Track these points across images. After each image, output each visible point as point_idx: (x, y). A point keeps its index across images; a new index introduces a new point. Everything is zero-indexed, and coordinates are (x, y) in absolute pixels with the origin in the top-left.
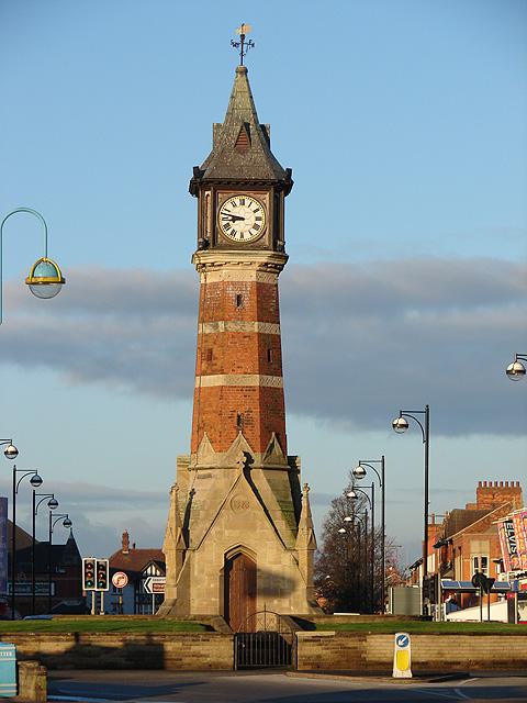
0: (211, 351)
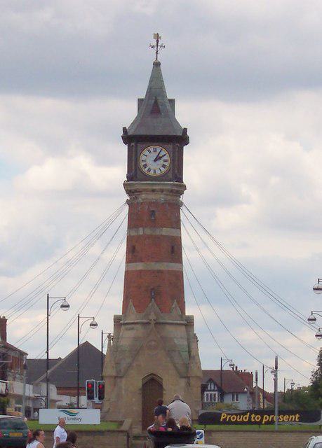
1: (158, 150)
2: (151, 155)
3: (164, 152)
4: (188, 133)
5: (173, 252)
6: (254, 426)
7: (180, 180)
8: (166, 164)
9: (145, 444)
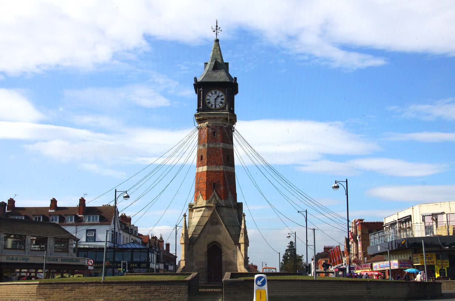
0: (202, 156)
1: (218, 92)
2: (213, 96)
3: (221, 94)
4: (235, 113)
5: (228, 159)
6: (376, 256)
7: (232, 111)
8: (223, 101)
9: (375, 276)
